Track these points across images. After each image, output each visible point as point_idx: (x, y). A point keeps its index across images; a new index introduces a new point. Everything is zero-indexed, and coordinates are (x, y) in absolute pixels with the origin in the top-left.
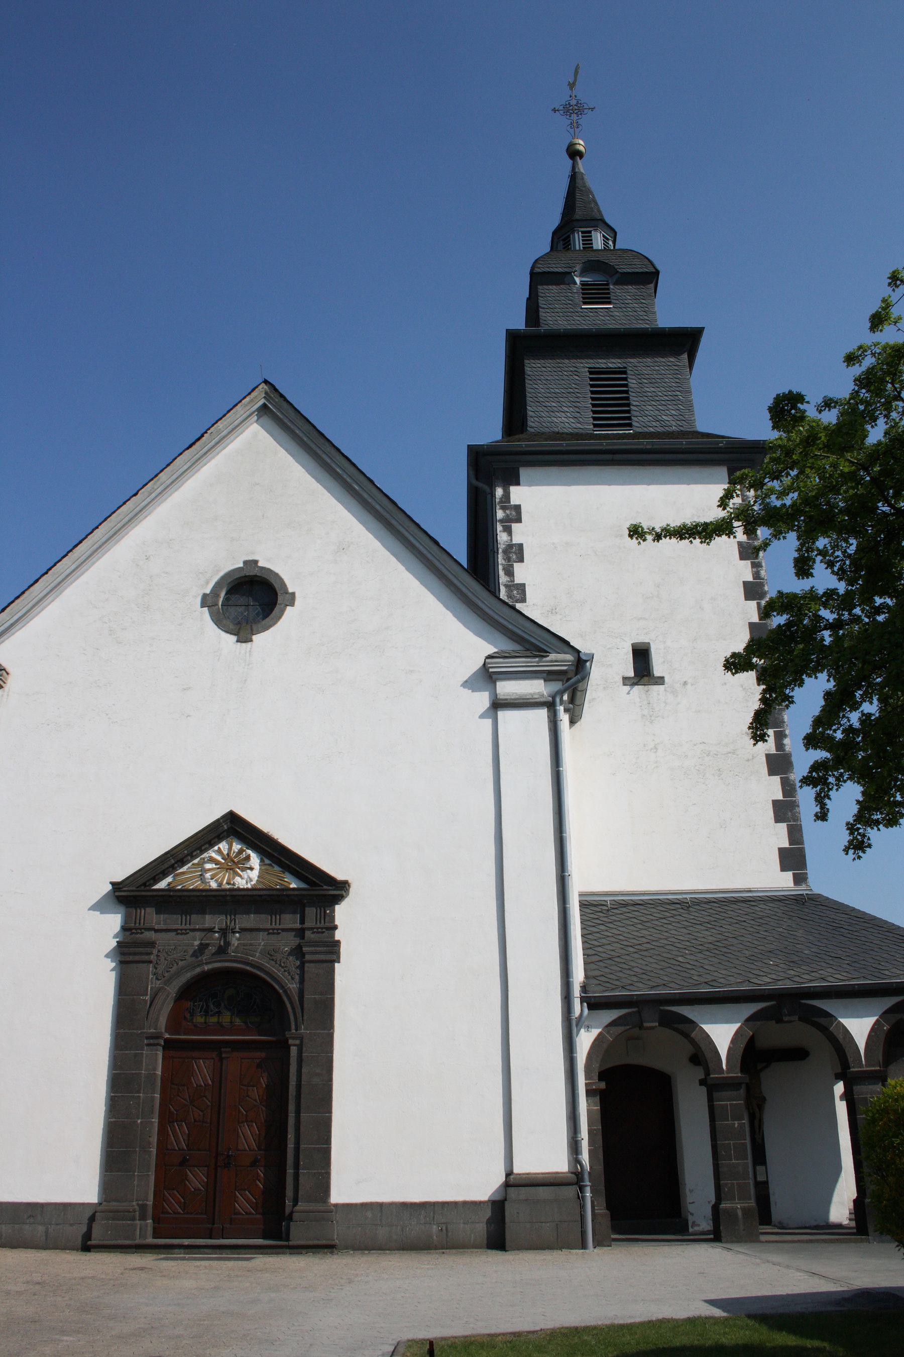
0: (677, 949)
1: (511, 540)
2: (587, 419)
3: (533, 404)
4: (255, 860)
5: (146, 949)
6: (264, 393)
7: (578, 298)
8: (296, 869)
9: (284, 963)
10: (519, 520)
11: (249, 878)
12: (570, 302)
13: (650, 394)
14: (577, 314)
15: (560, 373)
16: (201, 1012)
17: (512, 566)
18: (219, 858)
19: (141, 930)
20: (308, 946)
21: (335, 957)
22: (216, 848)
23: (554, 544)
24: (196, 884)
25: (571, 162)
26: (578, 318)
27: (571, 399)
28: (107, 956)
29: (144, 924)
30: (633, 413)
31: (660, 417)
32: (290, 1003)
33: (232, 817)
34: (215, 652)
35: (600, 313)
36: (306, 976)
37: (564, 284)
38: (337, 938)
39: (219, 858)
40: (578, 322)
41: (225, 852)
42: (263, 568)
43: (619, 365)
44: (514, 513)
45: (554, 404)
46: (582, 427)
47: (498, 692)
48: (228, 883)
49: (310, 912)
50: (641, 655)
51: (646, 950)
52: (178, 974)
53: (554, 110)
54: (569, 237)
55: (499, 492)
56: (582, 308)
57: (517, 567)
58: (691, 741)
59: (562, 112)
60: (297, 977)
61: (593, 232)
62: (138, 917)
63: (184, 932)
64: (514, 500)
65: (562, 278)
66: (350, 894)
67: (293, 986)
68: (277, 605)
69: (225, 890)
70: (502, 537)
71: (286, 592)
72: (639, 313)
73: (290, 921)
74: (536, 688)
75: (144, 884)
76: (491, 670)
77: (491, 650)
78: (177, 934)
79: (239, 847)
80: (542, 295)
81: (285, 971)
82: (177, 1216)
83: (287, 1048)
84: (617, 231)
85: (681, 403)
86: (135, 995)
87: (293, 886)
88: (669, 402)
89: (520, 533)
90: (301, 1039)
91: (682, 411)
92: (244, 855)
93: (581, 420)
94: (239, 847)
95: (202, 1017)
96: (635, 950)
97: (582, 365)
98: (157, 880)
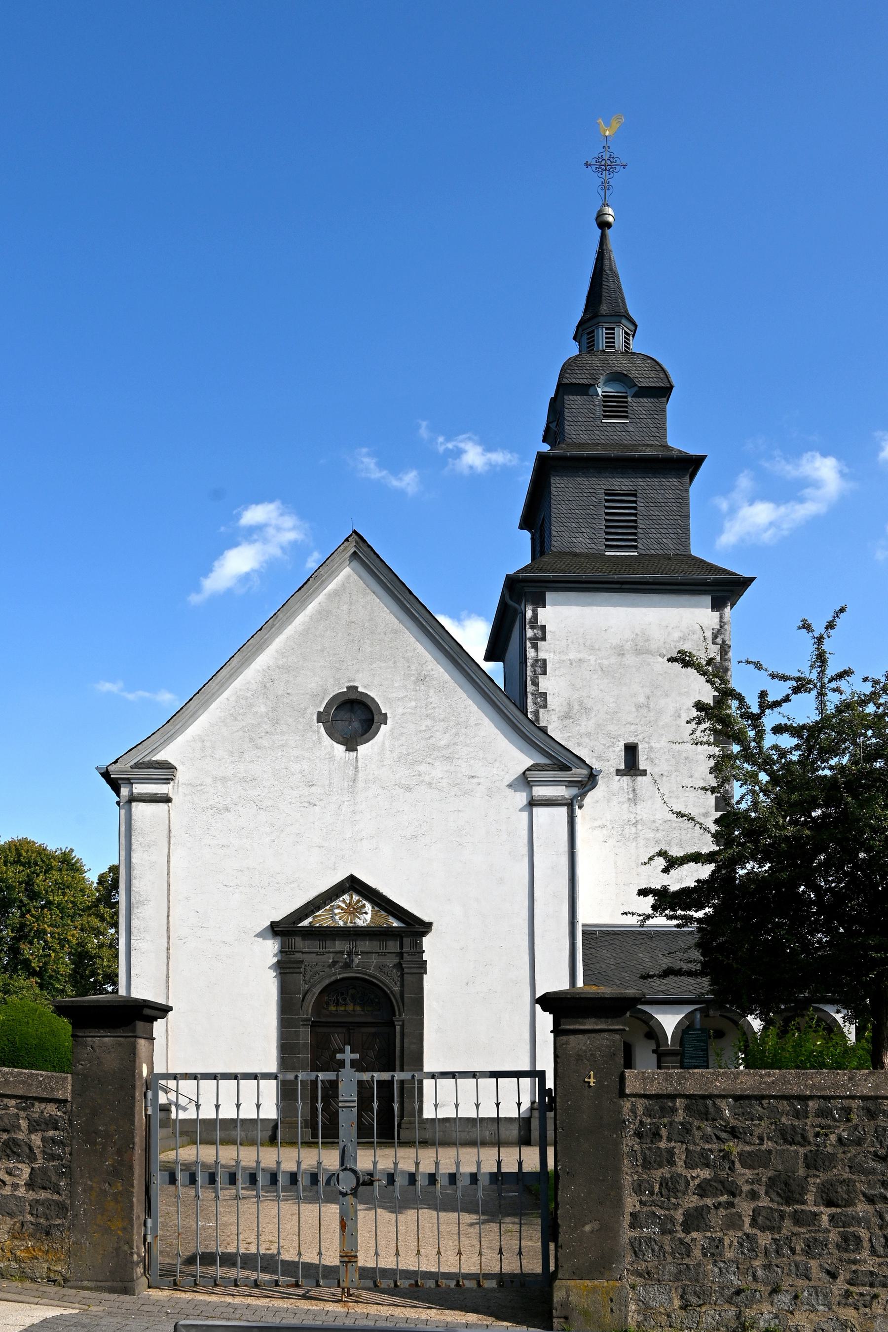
4: (368, 907)
7: (599, 411)
10: (544, 639)
12: (592, 415)
13: (654, 517)
15: (581, 494)
18: (344, 906)
19: (293, 953)
21: (423, 971)
22: (341, 899)
24: (327, 923)
25: (600, 231)
26: (598, 433)
28: (270, 968)
30: (639, 535)
33: (352, 879)
35: (618, 429)
36: (405, 983)
37: (587, 395)
39: (344, 906)
43: (631, 487)
44: (540, 632)
49: (407, 941)
50: (631, 750)
52: (320, 982)
53: (587, 165)
54: (593, 332)
55: (529, 614)
56: (602, 422)
57: (541, 679)
59: (594, 167)
60: (399, 983)
63: (323, 954)
64: (541, 621)
65: (585, 389)
67: (396, 989)
70: (531, 653)
73: (393, 946)
74: (560, 792)
75: (294, 923)
76: (529, 779)
77: (529, 762)
79: (357, 898)
83: (394, 1027)
87: (395, 925)
88: (669, 526)
89: (545, 651)
90: (403, 1021)
93: (595, 540)
94: (357, 898)
98: (301, 920)
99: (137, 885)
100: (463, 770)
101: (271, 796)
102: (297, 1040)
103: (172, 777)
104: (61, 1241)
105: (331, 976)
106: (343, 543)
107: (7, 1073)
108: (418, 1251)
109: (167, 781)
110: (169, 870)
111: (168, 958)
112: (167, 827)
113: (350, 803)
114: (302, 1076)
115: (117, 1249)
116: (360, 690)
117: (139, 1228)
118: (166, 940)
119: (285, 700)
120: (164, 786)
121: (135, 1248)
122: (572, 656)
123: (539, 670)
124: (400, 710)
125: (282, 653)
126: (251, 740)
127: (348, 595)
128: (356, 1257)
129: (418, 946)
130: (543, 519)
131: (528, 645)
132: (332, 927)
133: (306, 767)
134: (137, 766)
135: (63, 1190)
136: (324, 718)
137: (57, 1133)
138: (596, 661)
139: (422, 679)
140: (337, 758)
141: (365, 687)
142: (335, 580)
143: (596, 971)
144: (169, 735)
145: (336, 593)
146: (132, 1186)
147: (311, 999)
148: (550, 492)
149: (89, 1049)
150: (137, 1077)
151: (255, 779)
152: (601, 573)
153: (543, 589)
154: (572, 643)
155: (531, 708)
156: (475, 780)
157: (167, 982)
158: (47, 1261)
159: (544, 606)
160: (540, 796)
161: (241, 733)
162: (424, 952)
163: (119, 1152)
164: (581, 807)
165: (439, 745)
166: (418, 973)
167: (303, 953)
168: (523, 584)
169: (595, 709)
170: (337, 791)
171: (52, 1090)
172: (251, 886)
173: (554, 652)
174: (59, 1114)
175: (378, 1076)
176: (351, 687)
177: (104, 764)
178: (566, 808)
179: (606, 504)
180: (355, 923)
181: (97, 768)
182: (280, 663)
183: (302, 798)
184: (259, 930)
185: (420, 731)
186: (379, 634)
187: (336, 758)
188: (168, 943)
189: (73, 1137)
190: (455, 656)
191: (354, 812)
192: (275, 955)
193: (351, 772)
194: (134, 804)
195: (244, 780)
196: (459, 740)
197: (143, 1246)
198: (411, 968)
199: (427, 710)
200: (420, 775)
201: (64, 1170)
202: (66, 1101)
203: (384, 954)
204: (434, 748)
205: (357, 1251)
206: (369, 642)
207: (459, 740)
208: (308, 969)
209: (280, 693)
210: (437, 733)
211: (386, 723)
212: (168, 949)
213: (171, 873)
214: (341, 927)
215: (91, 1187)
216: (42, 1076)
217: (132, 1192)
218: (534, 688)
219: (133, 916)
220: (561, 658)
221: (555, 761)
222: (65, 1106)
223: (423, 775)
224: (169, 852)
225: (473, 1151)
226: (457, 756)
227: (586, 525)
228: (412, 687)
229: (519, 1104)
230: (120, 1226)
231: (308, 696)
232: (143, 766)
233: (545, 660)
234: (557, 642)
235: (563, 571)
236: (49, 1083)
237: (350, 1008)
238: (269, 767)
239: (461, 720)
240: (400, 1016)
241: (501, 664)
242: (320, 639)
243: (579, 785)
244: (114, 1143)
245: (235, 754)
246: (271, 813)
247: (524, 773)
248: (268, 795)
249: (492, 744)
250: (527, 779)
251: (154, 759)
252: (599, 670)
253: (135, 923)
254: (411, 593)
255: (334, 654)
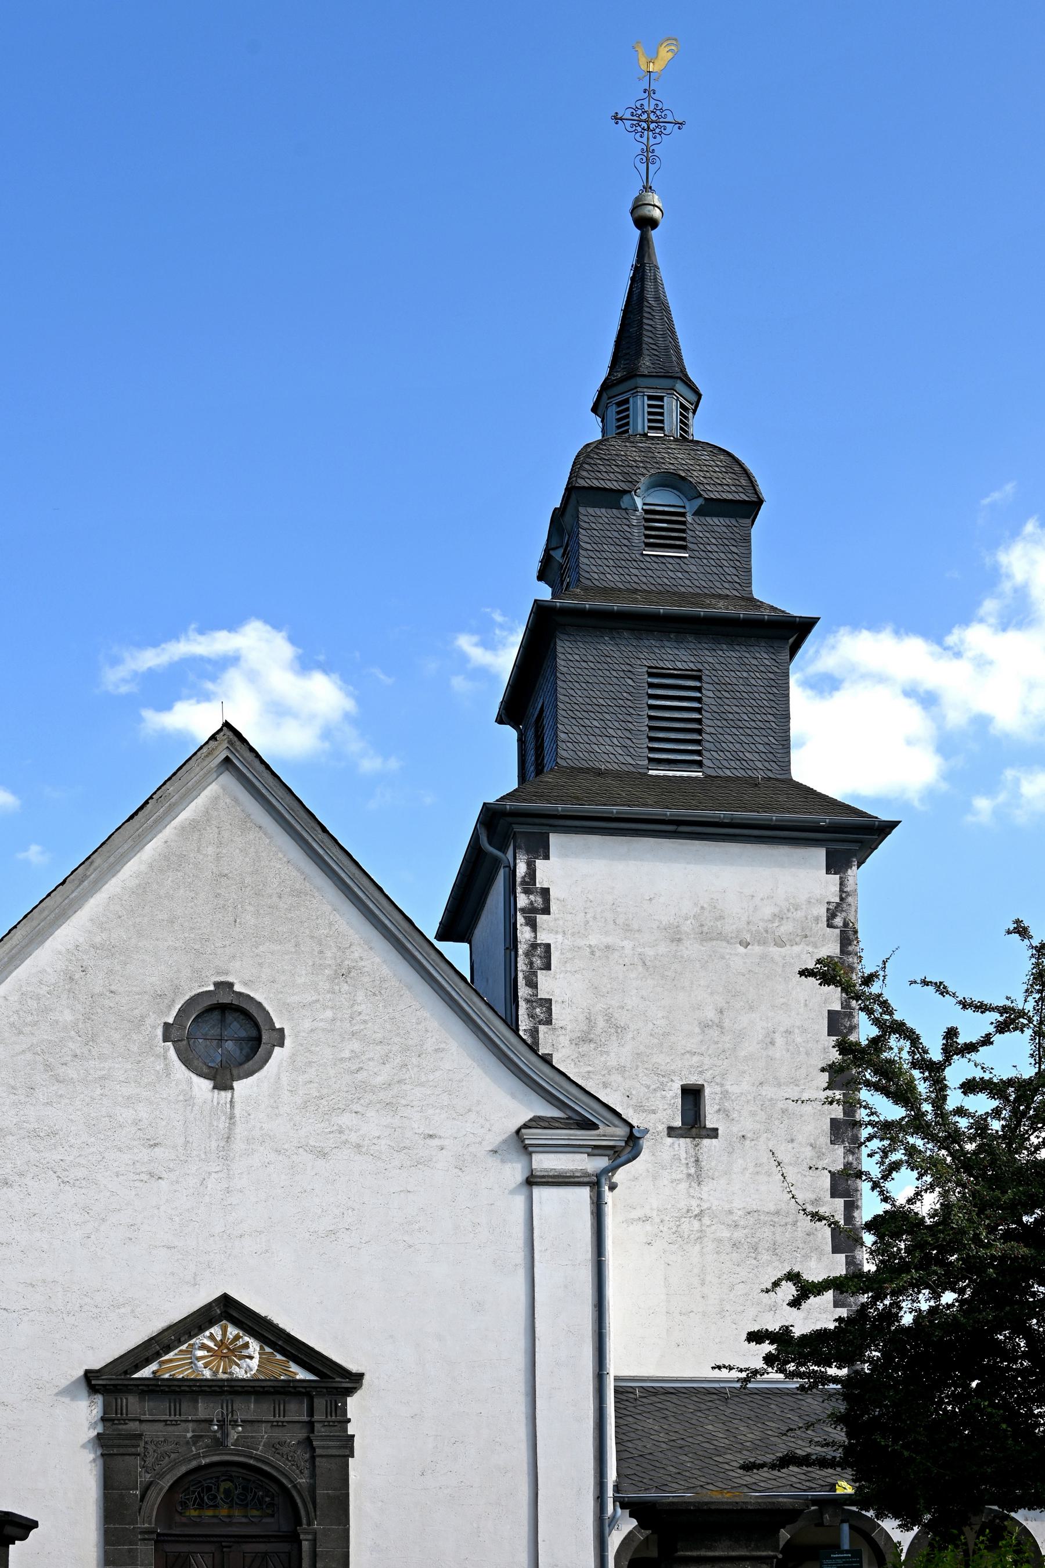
0: (714, 1447)
1: (536, 938)
2: (640, 750)
5: (133, 1441)
7: (637, 535)
8: (303, 1360)
9: (292, 1457)
11: (249, 1367)
12: (625, 542)
13: (731, 716)
14: (635, 563)
16: (193, 1505)
17: (535, 974)
18: (211, 1344)
20: (317, 1440)
22: (207, 1333)
25: (638, 232)
27: (620, 716)
28: (84, 1446)
29: (127, 1415)
31: (741, 754)
32: (300, 1498)
34: (186, 1101)
35: (670, 566)
36: (318, 1471)
39: (211, 1344)
40: (636, 579)
41: (219, 1338)
42: (240, 994)
44: (539, 900)
45: (596, 723)
46: (632, 762)
47: (534, 1167)
48: (224, 1373)
49: (320, 1403)
50: (692, 1095)
51: (680, 1448)
54: (627, 401)
56: (642, 554)
57: (542, 976)
58: (744, 1208)
60: (306, 1472)
61: (665, 398)
62: (119, 1407)
63: (176, 1423)
66: (363, 1387)
68: (262, 1045)
69: (222, 1380)
71: (272, 1027)
72: (726, 569)
73: (296, 1411)
75: (126, 1373)
76: (527, 1142)
78: (166, 1425)
80: (586, 526)
81: (293, 1465)
84: (701, 392)
85: (773, 734)
91: (773, 746)
92: (240, 1342)
93: (632, 750)
95: (195, 1511)
96: (669, 1447)
97: (639, 662)
98: (138, 1368)
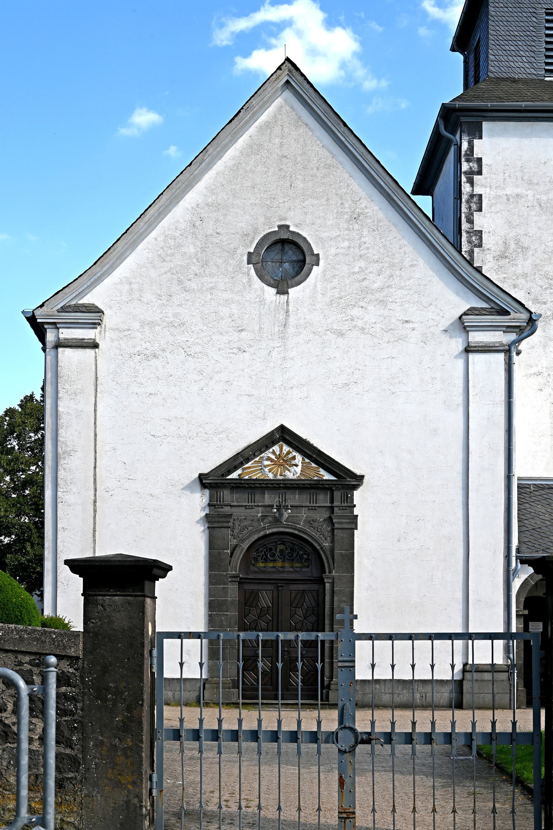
1: (473, 190)
2: (540, 64)
3: (494, 47)
4: (299, 458)
5: (226, 519)
6: (287, 70)
10: (480, 173)
11: (295, 471)
17: (472, 214)
18: (273, 457)
19: (222, 506)
22: (271, 450)
23: (507, 195)
28: (198, 522)
29: (223, 502)
33: (282, 429)
34: (260, 302)
36: (336, 538)
38: (355, 513)
39: (273, 457)
41: (278, 453)
44: (476, 166)
45: (512, 48)
49: (337, 495)
55: (465, 146)
60: (329, 539)
62: (219, 497)
63: (251, 507)
64: (477, 153)
66: (364, 484)
69: (280, 480)
70: (466, 188)
71: (312, 254)
73: (323, 500)
75: (223, 475)
76: (466, 324)
77: (465, 307)
78: (246, 508)
81: (321, 534)
82: (252, 686)
86: (220, 549)
92: (290, 456)
93: (534, 64)
97: (540, 6)
98: (230, 472)
99: (64, 434)
100: (398, 315)
101: (200, 342)
102: (226, 597)
103: (99, 321)
104: (74, 794)
105: (260, 531)
106: (275, 72)
107: (22, 630)
108: (414, 808)
109: (94, 325)
110: (95, 419)
111: (95, 511)
112: (94, 374)
113: (280, 349)
114: (302, 635)
115: (127, 802)
116: (292, 229)
117: (146, 783)
118: (92, 492)
119: (215, 240)
120: (91, 330)
121: (144, 801)
122: (509, 191)
123: (474, 206)
124: (333, 251)
125: (211, 190)
126: (180, 282)
127: (281, 128)
128: (354, 813)
129: (349, 500)
130: (479, 41)
131: (464, 179)
132: (262, 480)
133: (235, 311)
134: (63, 309)
135: (76, 745)
136: (254, 259)
137: (69, 689)
138: (533, 196)
139: (356, 218)
140: (268, 302)
141: (296, 226)
142: (267, 112)
143: (530, 527)
144: (96, 277)
145: (267, 125)
146: (142, 741)
147: (239, 555)
148: (487, 13)
149: (100, 607)
150: (145, 635)
151: (183, 324)
152: (543, 100)
153: (479, 119)
154: (510, 176)
155: (465, 247)
156: (410, 325)
157: (94, 536)
158: (61, 813)
159: (481, 137)
160: (477, 342)
161: (169, 275)
162: (355, 506)
163: (129, 709)
164: (518, 353)
165: (372, 287)
166: (348, 529)
167: (231, 506)
168: (458, 114)
169: (532, 247)
170: (267, 337)
171: (65, 648)
172: (179, 436)
173: (491, 187)
174: (71, 670)
175: (303, 636)
176: (283, 225)
177: (31, 307)
178: (503, 354)
179: (547, 25)
180: (285, 476)
181: (23, 312)
182: (210, 200)
183: (231, 344)
184: (187, 482)
185: (354, 273)
186: (312, 169)
187: (266, 301)
188: (95, 495)
189: (84, 694)
190: (390, 192)
191: (284, 359)
192: (203, 509)
193: (281, 316)
194: (60, 350)
195: (171, 325)
196: (393, 283)
197: (148, 800)
198: (342, 523)
199: (360, 251)
200: (352, 320)
201: (76, 725)
202: (78, 658)
203: (313, 509)
204: (367, 291)
205: (354, 808)
206: (301, 177)
207: (393, 283)
208: (237, 523)
209: (210, 232)
210: (371, 275)
211: (318, 264)
212: (95, 502)
213: (97, 423)
214: (270, 480)
215: (102, 743)
216: (54, 633)
217: (142, 748)
218: (469, 225)
219: (60, 467)
220: (498, 194)
221: (493, 305)
222: (77, 663)
223: (356, 320)
224: (96, 401)
225: (408, 713)
226: (391, 300)
227: (525, 48)
228: (345, 226)
229: (453, 666)
230: (130, 780)
231: (238, 236)
232: (69, 310)
233: (480, 196)
234: (494, 176)
235: (500, 99)
236: (62, 641)
237: (279, 564)
238: (197, 311)
239: (396, 261)
240: (330, 572)
241: (430, 198)
242: (250, 175)
243: (518, 330)
244: (124, 699)
245: (163, 298)
246: (199, 360)
247: (460, 318)
248: (196, 341)
249: (427, 287)
250: (463, 324)
251: (81, 302)
252: (538, 205)
253: (61, 474)
254: (345, 125)
255: (265, 191)
